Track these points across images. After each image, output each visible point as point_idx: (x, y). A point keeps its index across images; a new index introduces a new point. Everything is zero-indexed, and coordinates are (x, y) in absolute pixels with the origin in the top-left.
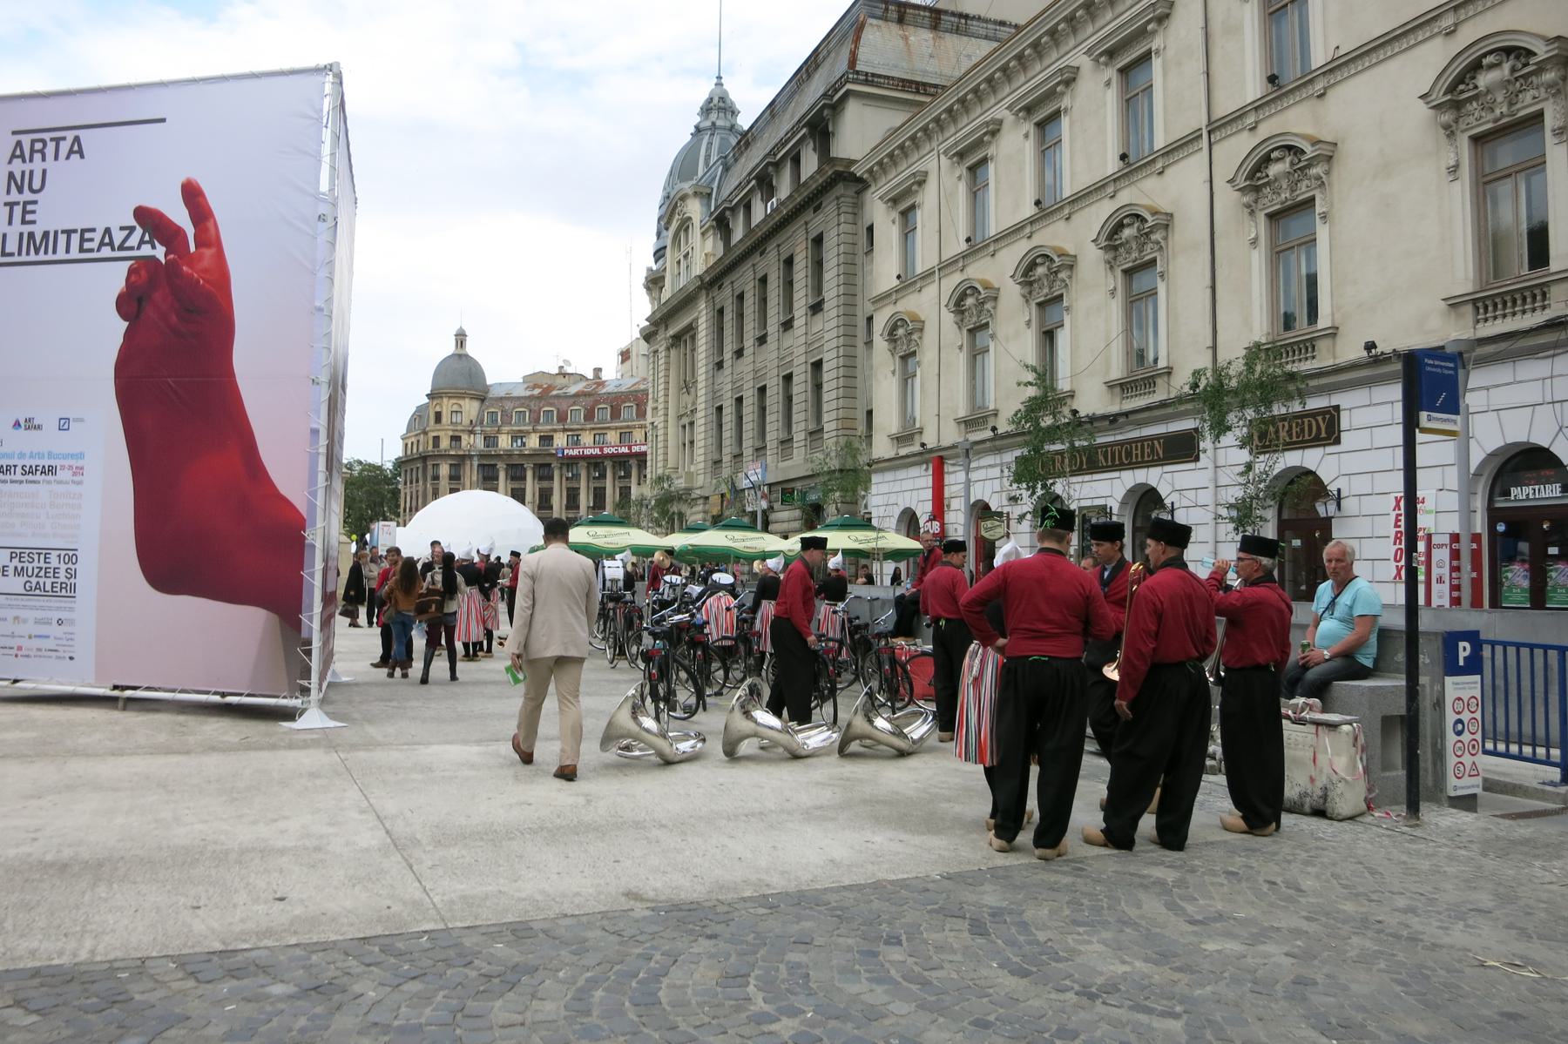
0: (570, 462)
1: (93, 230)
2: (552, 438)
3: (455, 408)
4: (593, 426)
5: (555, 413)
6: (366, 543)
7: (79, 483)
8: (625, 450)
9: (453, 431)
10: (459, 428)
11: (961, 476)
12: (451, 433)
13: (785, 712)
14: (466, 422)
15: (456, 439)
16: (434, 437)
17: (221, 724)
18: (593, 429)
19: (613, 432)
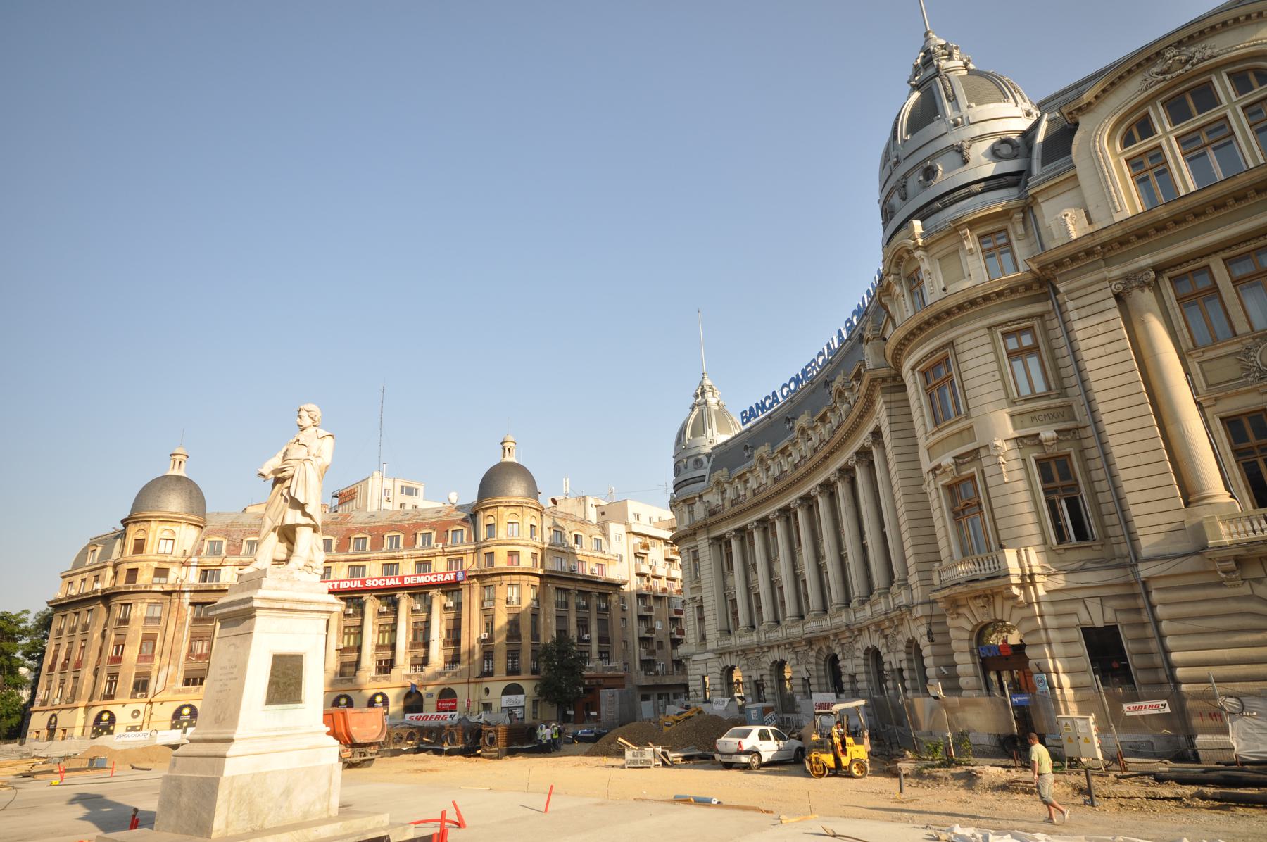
0: (420, 592)
1: (27, 612)
2: (430, 563)
3: (166, 535)
4: (348, 557)
5: (225, 543)
6: (820, 742)
7: (402, 492)
8: (358, 585)
9: (160, 562)
10: (169, 558)
11: (177, 600)
12: (156, 565)
13: (650, 744)
14: (178, 552)
15: (161, 572)
16: (129, 570)
17: (453, 763)
18: (348, 561)
19: (373, 564)
